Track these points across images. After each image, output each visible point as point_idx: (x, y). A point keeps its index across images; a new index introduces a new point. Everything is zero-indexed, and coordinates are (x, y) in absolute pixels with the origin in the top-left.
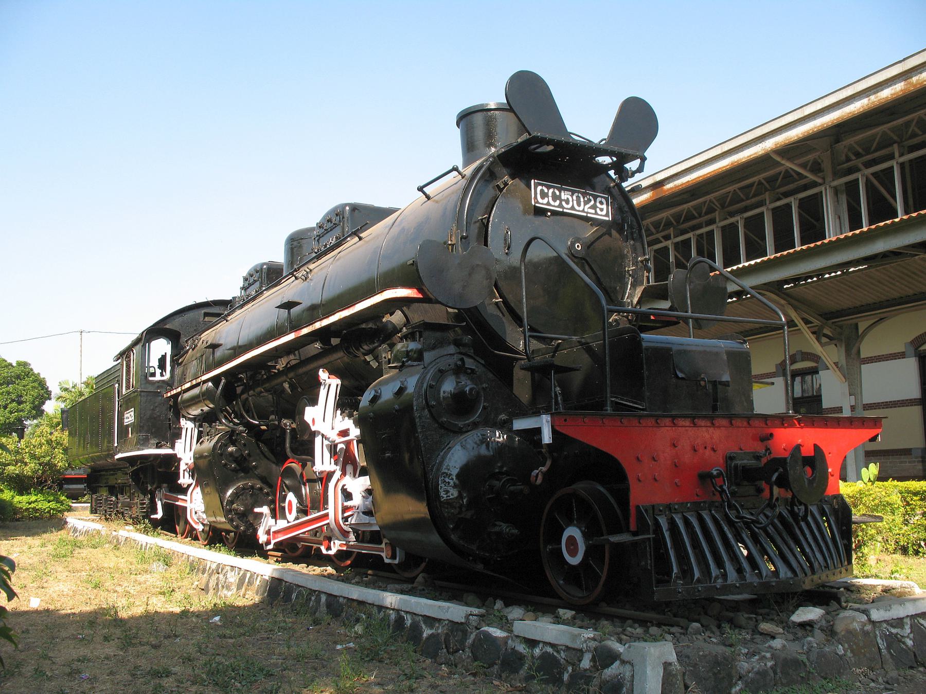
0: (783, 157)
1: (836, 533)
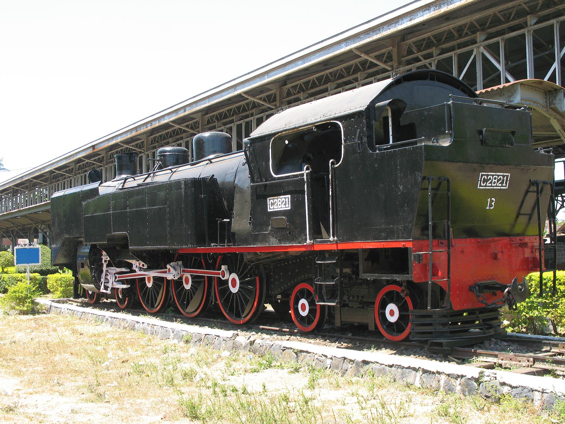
0: (361, 52)
1: (240, 295)
